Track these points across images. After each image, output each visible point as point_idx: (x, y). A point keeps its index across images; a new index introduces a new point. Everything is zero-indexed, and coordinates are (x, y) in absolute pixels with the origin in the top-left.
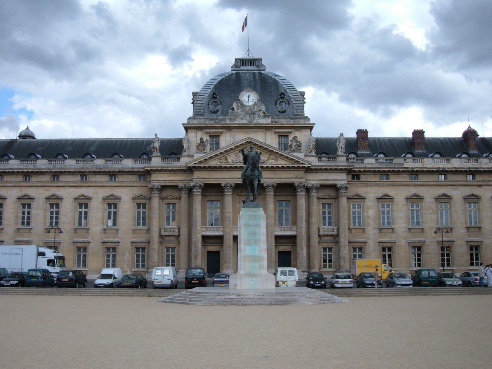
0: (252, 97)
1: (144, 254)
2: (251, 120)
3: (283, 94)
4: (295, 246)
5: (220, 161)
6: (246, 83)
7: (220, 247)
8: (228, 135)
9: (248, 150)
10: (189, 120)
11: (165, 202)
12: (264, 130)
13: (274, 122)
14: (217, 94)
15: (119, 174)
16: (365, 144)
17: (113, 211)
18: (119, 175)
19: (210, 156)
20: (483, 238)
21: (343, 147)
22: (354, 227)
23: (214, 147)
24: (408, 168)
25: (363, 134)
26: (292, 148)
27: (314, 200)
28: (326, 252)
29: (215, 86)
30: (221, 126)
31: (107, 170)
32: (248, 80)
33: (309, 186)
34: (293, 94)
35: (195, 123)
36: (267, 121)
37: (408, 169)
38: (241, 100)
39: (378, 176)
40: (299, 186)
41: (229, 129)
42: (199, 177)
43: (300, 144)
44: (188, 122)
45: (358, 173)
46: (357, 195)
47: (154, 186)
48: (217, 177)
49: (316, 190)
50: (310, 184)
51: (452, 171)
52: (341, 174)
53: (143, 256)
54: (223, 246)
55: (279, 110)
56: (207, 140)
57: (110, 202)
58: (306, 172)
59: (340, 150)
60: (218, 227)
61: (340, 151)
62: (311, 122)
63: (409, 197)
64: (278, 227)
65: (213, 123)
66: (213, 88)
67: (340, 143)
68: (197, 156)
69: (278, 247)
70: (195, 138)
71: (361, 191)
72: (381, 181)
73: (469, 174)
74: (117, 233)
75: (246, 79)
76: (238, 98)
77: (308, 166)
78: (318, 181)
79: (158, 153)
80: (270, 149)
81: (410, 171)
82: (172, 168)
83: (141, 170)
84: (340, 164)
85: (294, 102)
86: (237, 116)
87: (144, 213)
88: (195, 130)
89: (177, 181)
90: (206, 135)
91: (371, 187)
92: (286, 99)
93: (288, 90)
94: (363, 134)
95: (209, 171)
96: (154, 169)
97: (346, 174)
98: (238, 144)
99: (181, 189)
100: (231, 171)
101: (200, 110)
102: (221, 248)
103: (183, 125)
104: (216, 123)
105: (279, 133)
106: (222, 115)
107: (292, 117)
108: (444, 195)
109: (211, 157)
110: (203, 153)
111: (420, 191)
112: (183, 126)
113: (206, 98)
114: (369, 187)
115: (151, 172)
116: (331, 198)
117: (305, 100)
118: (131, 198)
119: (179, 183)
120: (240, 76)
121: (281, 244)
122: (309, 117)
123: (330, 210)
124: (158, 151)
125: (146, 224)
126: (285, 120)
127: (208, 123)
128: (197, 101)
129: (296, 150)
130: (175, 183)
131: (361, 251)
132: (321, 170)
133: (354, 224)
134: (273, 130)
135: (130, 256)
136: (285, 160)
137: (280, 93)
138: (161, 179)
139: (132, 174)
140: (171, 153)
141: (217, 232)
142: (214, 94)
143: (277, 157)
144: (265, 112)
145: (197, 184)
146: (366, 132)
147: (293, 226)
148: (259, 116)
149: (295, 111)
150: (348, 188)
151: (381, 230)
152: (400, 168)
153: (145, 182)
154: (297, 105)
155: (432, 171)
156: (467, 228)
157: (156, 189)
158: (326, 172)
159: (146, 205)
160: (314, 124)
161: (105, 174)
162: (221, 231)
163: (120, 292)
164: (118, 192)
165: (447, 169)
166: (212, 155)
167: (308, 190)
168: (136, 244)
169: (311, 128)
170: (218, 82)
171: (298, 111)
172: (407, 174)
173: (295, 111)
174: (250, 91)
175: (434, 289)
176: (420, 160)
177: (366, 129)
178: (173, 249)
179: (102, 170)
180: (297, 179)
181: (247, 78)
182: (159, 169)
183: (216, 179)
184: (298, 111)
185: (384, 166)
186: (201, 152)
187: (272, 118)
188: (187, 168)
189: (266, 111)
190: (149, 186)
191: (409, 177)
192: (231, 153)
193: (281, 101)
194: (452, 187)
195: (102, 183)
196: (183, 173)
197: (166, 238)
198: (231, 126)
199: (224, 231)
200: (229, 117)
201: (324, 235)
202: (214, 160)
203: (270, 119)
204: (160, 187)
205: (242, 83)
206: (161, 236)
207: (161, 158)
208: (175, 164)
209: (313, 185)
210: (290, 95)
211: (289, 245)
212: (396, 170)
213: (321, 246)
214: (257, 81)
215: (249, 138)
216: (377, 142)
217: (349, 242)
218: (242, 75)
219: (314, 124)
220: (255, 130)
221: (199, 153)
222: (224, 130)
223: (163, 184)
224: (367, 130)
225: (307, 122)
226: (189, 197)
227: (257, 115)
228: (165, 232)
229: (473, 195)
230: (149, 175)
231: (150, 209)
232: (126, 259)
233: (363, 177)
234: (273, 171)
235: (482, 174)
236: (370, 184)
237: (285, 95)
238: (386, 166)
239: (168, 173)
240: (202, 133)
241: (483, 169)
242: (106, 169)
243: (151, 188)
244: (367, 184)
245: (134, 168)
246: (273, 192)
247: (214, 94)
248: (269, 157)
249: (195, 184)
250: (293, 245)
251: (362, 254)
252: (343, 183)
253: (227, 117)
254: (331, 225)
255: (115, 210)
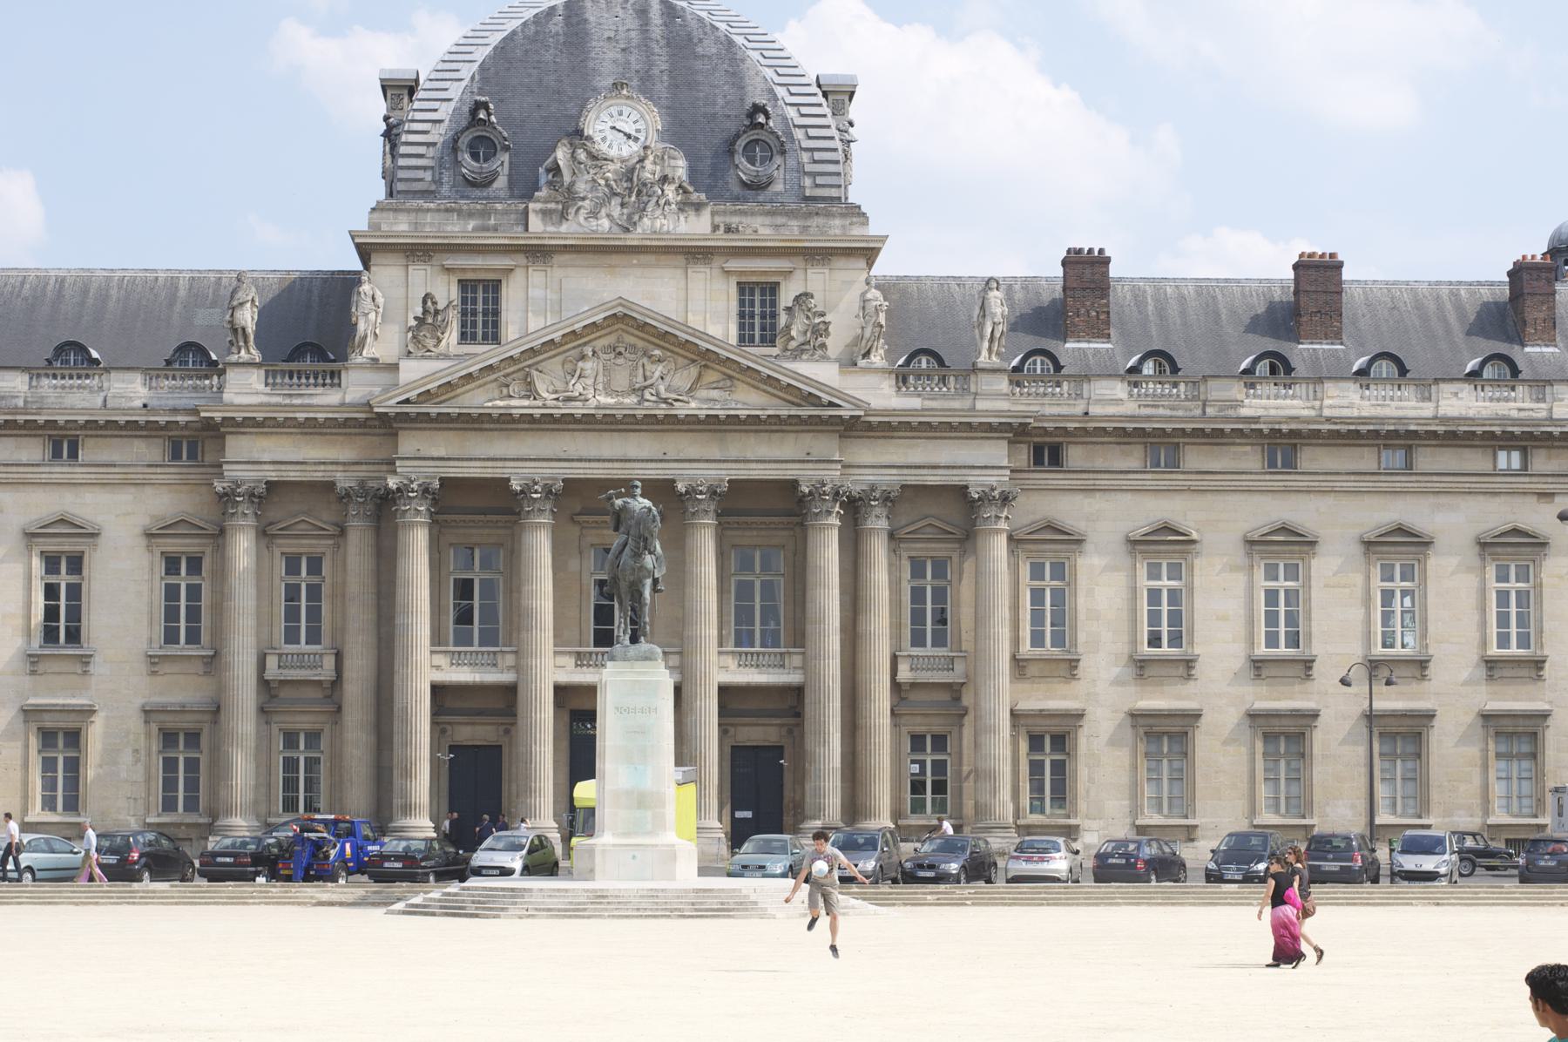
0: (635, 122)
1: (196, 755)
2: (630, 217)
3: (758, 109)
4: (797, 725)
5: (505, 391)
6: (611, 55)
7: (502, 728)
8: (537, 276)
9: (618, 350)
10: (376, 215)
11: (279, 546)
12: (681, 260)
13: (722, 229)
14: (491, 106)
15: (90, 433)
16: (1094, 314)
17: (67, 584)
18: (91, 436)
19: (464, 373)
20: (1550, 703)
21: (997, 335)
22: (1038, 652)
23: (480, 324)
24: (1256, 420)
25: (1088, 271)
26: (793, 338)
27: (878, 551)
28: (925, 750)
29: (483, 68)
30: (507, 242)
31: (41, 419)
32: (617, 41)
33: (856, 489)
34: (804, 110)
35: (400, 227)
36: (696, 227)
37: (1257, 426)
38: (588, 131)
39: (1138, 451)
40: (817, 492)
41: (539, 253)
42: (422, 454)
43: (824, 322)
44: (374, 226)
45: (1057, 439)
46: (1051, 527)
47: (239, 486)
48: (491, 455)
49: (886, 505)
50: (857, 482)
51: (1434, 434)
52: (988, 442)
53: (192, 765)
54: (513, 724)
55: (744, 178)
56: (450, 302)
57: (52, 546)
58: (847, 434)
59: (986, 344)
60: (495, 653)
61: (985, 353)
62: (873, 229)
63: (1256, 538)
64: (732, 652)
65: (475, 229)
66: (473, 78)
67: (984, 316)
68: (414, 372)
69: (732, 730)
70: (403, 290)
71: (1069, 509)
72: (1148, 472)
73: (1509, 448)
74: (85, 673)
75: (609, 38)
76: (577, 124)
77: (852, 417)
78: (894, 471)
79: (252, 351)
80: (704, 345)
81: (1266, 431)
82: (312, 415)
83: (181, 419)
84: (981, 405)
85: (807, 144)
86: (568, 199)
87: (194, 592)
88: (402, 255)
89: (330, 468)
90: (446, 277)
91: (1107, 493)
92: (773, 133)
93: (781, 92)
94: (1088, 271)
95: (461, 429)
96: (239, 416)
97: (1005, 443)
98: (578, 326)
99: (347, 496)
100: (548, 430)
101: (420, 174)
102: (507, 732)
103: (353, 238)
104: (485, 229)
105: (742, 273)
106: (512, 197)
107: (794, 206)
108: (1400, 530)
109: (469, 377)
110: (437, 357)
111: (1303, 512)
112: (353, 239)
113: (447, 122)
114: (1098, 495)
115: (222, 430)
116: (945, 536)
117: (851, 129)
118: (139, 530)
119: (339, 474)
120: (586, 20)
121: (747, 720)
122: (863, 209)
123: (941, 583)
124: (251, 343)
125: (205, 637)
126: (768, 220)
127: (459, 229)
128: (413, 121)
129: (807, 347)
130: (320, 474)
131: (1064, 750)
132: (908, 426)
133: (1037, 639)
134: (718, 261)
135: (140, 768)
136: (764, 391)
137: (748, 105)
138: (266, 458)
139: (145, 433)
140: (297, 348)
141: (494, 669)
142: (478, 106)
143: (730, 377)
144: (685, 184)
145: (412, 482)
146: (1101, 261)
147: (791, 650)
148: (662, 202)
149: (808, 182)
150: (1014, 498)
151: (1141, 667)
152: (1227, 419)
153: (198, 466)
154: (817, 156)
155: (1356, 434)
156: (1487, 662)
157: (246, 497)
158: (925, 434)
159: (201, 558)
160: (883, 239)
161: (34, 432)
162: (509, 668)
163: (245, 892)
164: (89, 505)
165: (1412, 428)
166: (471, 370)
167: (854, 507)
168: (162, 717)
169: (869, 254)
170: (496, 48)
171: (819, 180)
172: (1252, 444)
173: (808, 182)
174: (628, 98)
175: (1126, 887)
176: (1311, 387)
177: (1101, 251)
178: (313, 738)
179: (21, 418)
180: (810, 466)
181: (612, 34)
182: (260, 416)
183: (490, 464)
184: (819, 180)
185: (1161, 411)
186: (429, 351)
187: (713, 214)
188: (374, 416)
189: (691, 183)
190: (219, 486)
191: (1260, 456)
192: (550, 358)
193: (751, 141)
194: (1432, 499)
195: (21, 469)
196: (356, 434)
197: (285, 693)
198: (546, 242)
199: (517, 668)
200: (539, 206)
201: (914, 685)
202: (480, 386)
203: (706, 216)
204: (262, 488)
205: (593, 55)
206: (264, 684)
207: (262, 372)
208: (325, 399)
209: (873, 488)
210: (791, 113)
211: (778, 721)
212: (1208, 427)
213: (904, 725)
214: (657, 50)
215: (622, 301)
216: (1149, 300)
217: (1012, 710)
218: (592, 19)
219: (883, 239)
220: (651, 258)
221: (416, 358)
222: (521, 259)
223: (272, 474)
224: (1107, 254)
225: (856, 231)
226: (378, 531)
227: (655, 199)
228: (279, 667)
229: (1516, 531)
230: (216, 437)
231: (222, 573)
232: (124, 775)
233: (1075, 456)
234: (715, 431)
235: (1554, 447)
236: (1104, 481)
237: (768, 117)
238: (1168, 412)
239: (291, 433)
240: (429, 268)
241: (1559, 429)
242: (40, 414)
243: (226, 494)
244: (1091, 482)
245: (154, 411)
246: (712, 514)
247: (478, 106)
248: (700, 375)
249: (406, 482)
250: (792, 721)
251: (1064, 761)
252: (992, 480)
253: (531, 206)
254: (945, 646)
255: (74, 579)
